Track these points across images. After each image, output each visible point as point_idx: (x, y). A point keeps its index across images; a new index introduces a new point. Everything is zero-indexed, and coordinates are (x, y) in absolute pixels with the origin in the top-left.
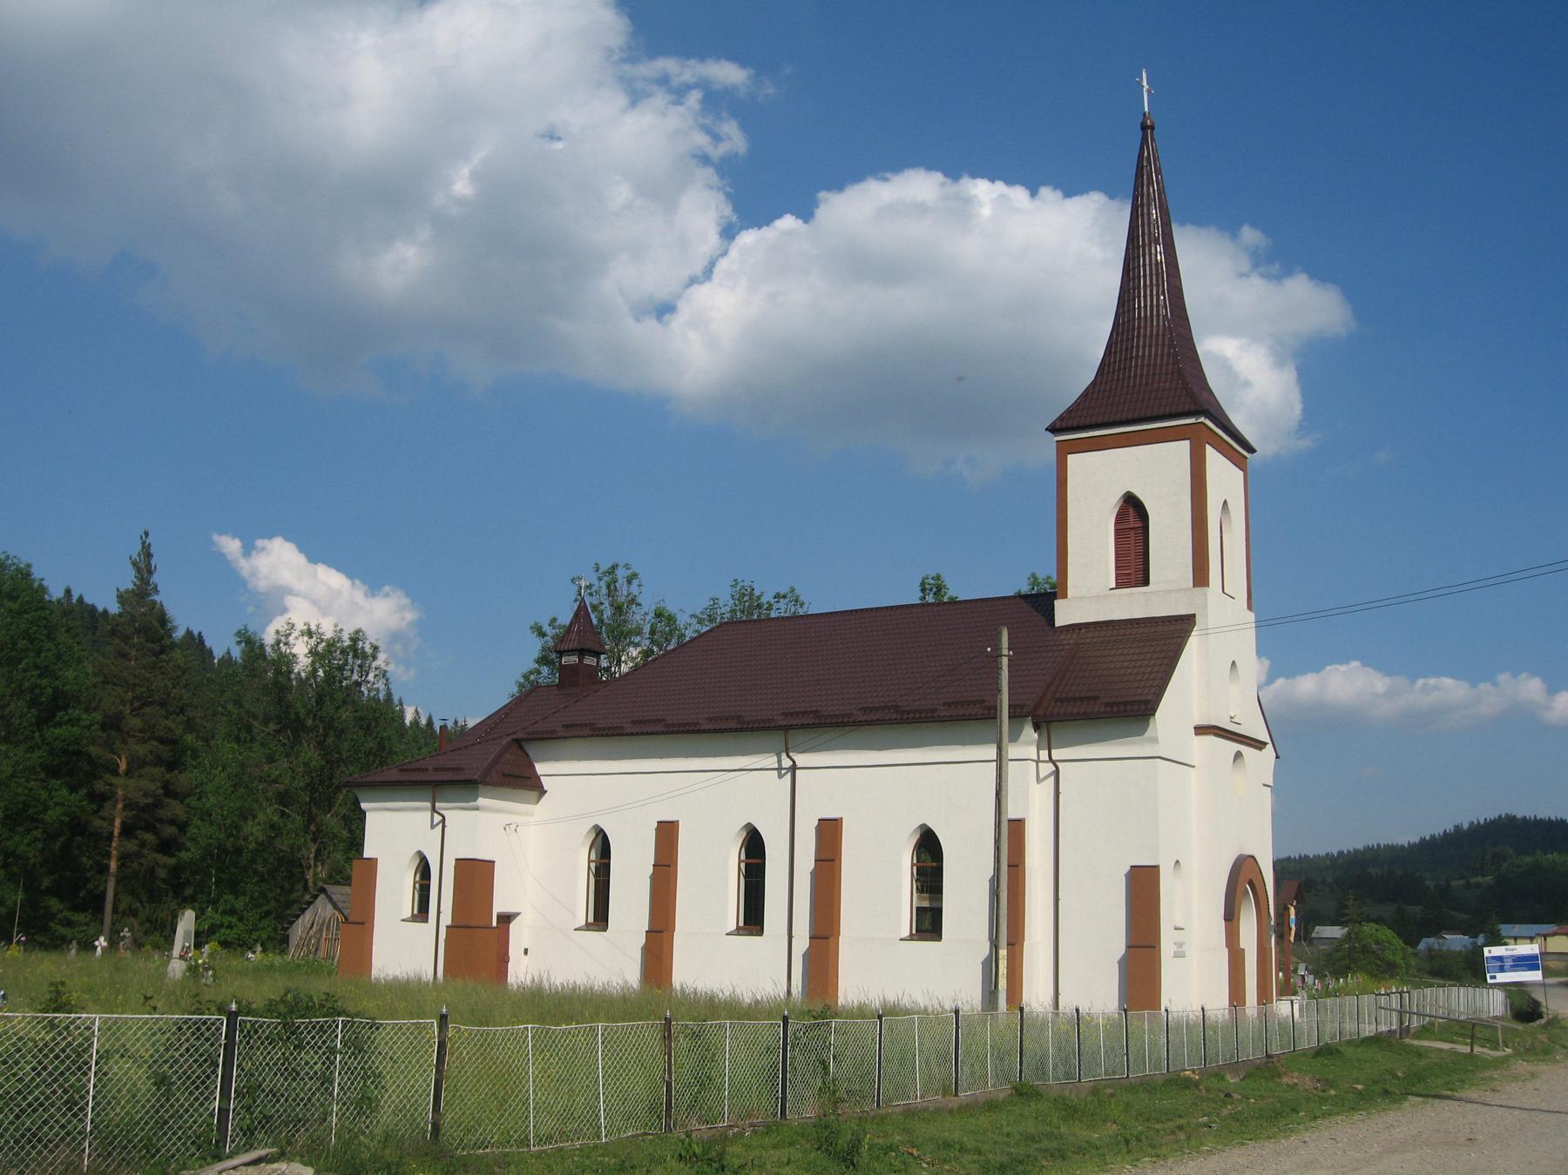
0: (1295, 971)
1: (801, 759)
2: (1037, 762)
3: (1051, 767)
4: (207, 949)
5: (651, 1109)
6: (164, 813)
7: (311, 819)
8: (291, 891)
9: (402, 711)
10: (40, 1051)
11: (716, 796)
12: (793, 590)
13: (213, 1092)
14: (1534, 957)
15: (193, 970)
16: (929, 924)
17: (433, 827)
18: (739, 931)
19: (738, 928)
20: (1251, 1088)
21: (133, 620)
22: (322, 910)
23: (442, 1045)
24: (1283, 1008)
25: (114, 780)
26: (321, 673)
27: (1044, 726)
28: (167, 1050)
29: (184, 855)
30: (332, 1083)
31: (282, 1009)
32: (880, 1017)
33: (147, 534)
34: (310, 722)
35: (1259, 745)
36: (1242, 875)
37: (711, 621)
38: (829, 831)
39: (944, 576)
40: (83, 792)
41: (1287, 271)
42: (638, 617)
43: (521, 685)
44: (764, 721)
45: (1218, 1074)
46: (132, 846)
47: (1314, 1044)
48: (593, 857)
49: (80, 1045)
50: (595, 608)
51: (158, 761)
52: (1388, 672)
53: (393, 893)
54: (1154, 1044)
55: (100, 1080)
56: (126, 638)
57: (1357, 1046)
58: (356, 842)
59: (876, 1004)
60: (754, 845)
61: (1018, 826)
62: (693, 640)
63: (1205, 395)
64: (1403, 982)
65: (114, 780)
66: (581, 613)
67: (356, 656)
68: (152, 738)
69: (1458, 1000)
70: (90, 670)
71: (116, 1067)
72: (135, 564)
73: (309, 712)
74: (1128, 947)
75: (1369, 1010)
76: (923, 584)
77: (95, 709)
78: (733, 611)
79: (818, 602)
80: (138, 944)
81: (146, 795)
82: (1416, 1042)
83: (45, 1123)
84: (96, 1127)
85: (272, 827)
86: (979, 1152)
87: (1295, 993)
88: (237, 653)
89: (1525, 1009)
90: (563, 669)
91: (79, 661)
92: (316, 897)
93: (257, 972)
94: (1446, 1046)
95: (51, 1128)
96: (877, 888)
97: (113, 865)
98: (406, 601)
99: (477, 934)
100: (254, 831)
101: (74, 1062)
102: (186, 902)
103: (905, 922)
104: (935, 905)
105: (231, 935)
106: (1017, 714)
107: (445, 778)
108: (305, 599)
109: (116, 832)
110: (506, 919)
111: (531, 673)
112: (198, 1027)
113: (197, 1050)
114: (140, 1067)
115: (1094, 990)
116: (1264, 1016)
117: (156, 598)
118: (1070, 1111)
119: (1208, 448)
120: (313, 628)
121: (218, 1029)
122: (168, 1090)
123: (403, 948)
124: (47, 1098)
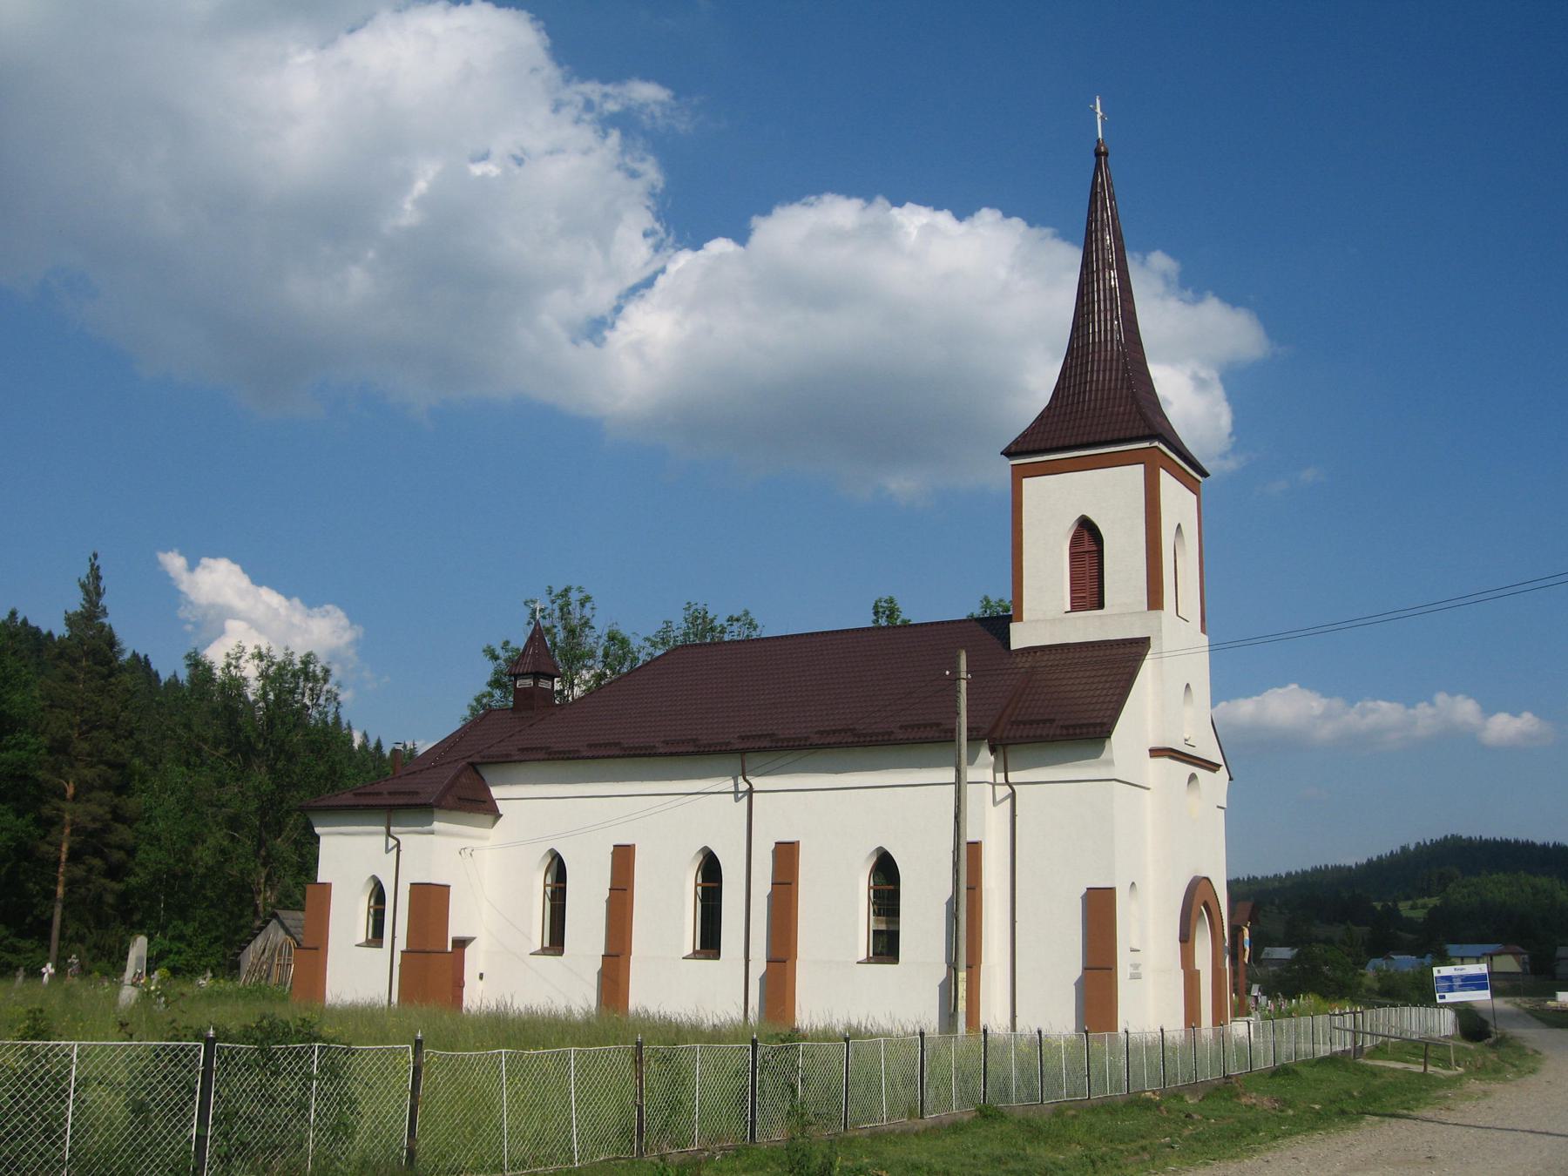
0: (1248, 992)
1: (758, 783)
2: (994, 784)
3: (1007, 790)
4: (156, 975)
5: (624, 1133)
6: (113, 839)
7: (261, 843)
8: (241, 917)
10: (19, 1078)
11: (672, 819)
12: (747, 613)
13: (190, 1119)
14: (1483, 977)
15: (146, 995)
16: (886, 947)
17: (387, 851)
18: (696, 955)
19: (695, 952)
20: (1229, 1105)
21: (81, 642)
22: (274, 935)
24: (1238, 1029)
25: (63, 805)
27: (1000, 749)
28: (145, 1077)
29: (133, 881)
30: (308, 1109)
31: (258, 1034)
32: (847, 1040)
33: (95, 556)
35: (1213, 767)
36: (1197, 897)
37: (663, 644)
38: (786, 855)
40: (30, 816)
41: (1198, 297)
42: (590, 640)
43: (473, 709)
45: (1177, 1095)
46: (79, 871)
48: (549, 881)
49: (59, 1072)
50: (548, 631)
51: (106, 785)
52: (1325, 694)
53: (347, 917)
55: (78, 1108)
56: (74, 662)
58: (307, 864)
59: (840, 1028)
60: (710, 868)
61: (975, 848)
62: (647, 664)
63: (1159, 419)
64: (1355, 1002)
65: (63, 805)
66: (537, 637)
67: (307, 680)
68: (100, 762)
69: (1410, 1020)
70: (37, 693)
71: (93, 1094)
72: (83, 586)
73: (260, 735)
74: (1085, 969)
75: (1323, 1030)
76: (876, 607)
77: (43, 733)
78: (686, 634)
79: (771, 627)
80: (85, 972)
81: (94, 820)
82: (1370, 1062)
83: (24, 1151)
84: (74, 1155)
85: (223, 851)
87: (1249, 1014)
88: (184, 675)
89: (1473, 1025)
90: (518, 693)
91: (26, 684)
92: (267, 922)
93: (210, 997)
94: (1399, 1065)
95: (30, 1156)
96: (834, 912)
97: (60, 890)
98: (345, 622)
99: (433, 959)
100: (204, 855)
101: (52, 1090)
102: (139, 927)
103: (861, 945)
105: (180, 961)
106: (975, 738)
107: (401, 802)
108: (238, 618)
109: (63, 857)
110: (461, 944)
111: (483, 696)
112: (176, 1055)
113: (174, 1077)
114: (118, 1094)
115: (1051, 1011)
116: (1221, 1038)
117: (106, 621)
118: (1035, 1132)
120: (264, 651)
121: (196, 1056)
122: (146, 1117)
123: (358, 974)
124: (26, 1126)
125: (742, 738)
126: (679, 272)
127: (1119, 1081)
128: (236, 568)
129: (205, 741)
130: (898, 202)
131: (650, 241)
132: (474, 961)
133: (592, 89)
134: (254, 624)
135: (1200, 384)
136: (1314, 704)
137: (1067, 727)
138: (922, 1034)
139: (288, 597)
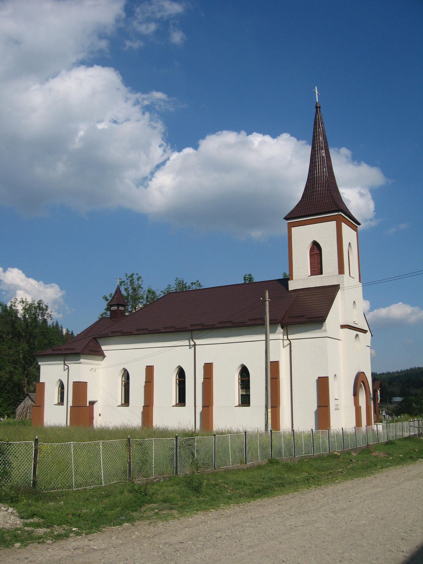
1: (197, 342)
2: (283, 340)
3: (288, 342)
7: (25, 369)
9: (62, 330)
11: (167, 356)
12: (198, 281)
16: (245, 400)
17: (65, 370)
18: (177, 405)
19: (176, 404)
22: (27, 402)
23: (36, 451)
24: (380, 427)
26: (27, 316)
27: (285, 327)
32: (215, 435)
34: (24, 334)
35: (365, 331)
36: (359, 380)
39: (252, 275)
42: (141, 293)
44: (184, 328)
45: (349, 453)
47: (386, 440)
48: (123, 380)
52: (412, 305)
53: (51, 395)
54: (323, 442)
57: (403, 440)
60: (181, 373)
67: (40, 310)
73: (23, 330)
74: (318, 407)
76: (245, 277)
78: (176, 289)
79: (206, 285)
85: (11, 372)
86: (251, 485)
90: (112, 312)
92: (25, 397)
96: (227, 388)
98: (59, 289)
99: (82, 408)
103: (237, 400)
104: (248, 393)
106: (274, 323)
110: (92, 403)
115: (306, 423)
118: (289, 468)
119: (343, 225)
120: (24, 300)
123: (55, 415)
125: (191, 325)
126: (174, 160)
127: (326, 448)
128: (20, 272)
129: (4, 333)
130: (249, 133)
131: (162, 148)
132: (97, 409)
133: (138, 95)
134: (26, 291)
135: (361, 195)
136: (408, 309)
137: (309, 318)
138: (245, 432)
139: (38, 280)
